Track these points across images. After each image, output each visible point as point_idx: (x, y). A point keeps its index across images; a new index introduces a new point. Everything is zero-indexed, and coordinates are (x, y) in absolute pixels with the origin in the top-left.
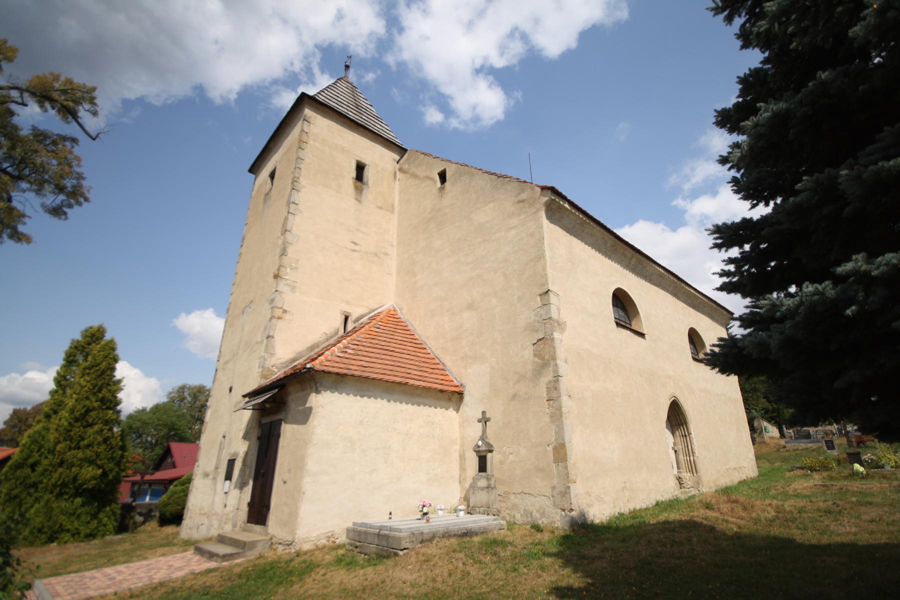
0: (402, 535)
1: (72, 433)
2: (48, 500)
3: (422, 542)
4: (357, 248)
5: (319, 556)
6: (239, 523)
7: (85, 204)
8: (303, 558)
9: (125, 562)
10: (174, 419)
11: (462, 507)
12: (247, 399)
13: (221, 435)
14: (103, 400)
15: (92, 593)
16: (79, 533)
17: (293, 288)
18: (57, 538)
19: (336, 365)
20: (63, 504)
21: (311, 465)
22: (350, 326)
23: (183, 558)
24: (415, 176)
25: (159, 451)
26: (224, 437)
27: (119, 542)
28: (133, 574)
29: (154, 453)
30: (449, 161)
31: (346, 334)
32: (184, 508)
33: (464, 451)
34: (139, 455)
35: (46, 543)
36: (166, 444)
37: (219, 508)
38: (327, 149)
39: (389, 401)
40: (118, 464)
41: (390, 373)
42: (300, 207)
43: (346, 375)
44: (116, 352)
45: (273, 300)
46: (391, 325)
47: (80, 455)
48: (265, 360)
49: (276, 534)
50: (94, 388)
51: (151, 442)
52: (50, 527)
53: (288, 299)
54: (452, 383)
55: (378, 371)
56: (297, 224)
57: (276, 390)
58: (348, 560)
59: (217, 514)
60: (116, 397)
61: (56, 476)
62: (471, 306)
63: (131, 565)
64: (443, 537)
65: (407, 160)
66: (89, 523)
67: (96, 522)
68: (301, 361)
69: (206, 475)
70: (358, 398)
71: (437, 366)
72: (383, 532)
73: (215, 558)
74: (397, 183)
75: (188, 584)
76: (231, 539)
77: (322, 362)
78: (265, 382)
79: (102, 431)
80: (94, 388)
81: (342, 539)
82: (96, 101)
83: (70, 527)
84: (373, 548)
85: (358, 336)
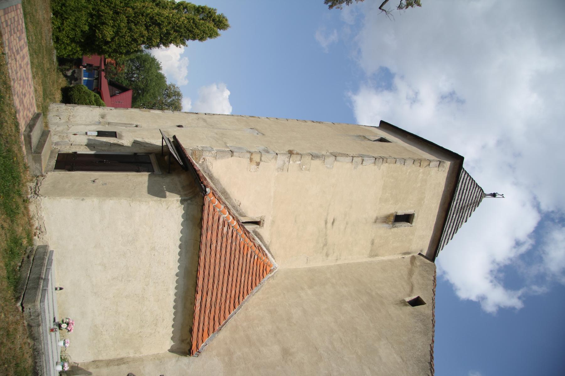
0: (38, 303)
1: (141, 17)
2: (87, 8)
3: (30, 326)
4: (329, 225)
5: (22, 221)
6: (59, 147)
7: (327, 6)
8: (22, 206)
9: (32, 63)
10: (152, 91)
11: (67, 368)
12: (172, 140)
13: (138, 124)
14: (168, 34)
15: (6, 37)
16: (60, 31)
17: (281, 169)
18: (57, 17)
19: (211, 217)
20: (84, 18)
21: (110, 204)
22: (249, 228)
23: (31, 104)
24: (411, 273)
25: (125, 83)
26: (137, 126)
27: (51, 60)
28: (21, 67)
29: (123, 80)
30: (434, 307)
31: (242, 225)
32: (75, 103)
33: (128, 362)
34: (122, 70)
35: (53, 10)
36: (130, 88)
37: (73, 130)
38: (419, 185)
39: (177, 275)
40: (115, 51)
41: (207, 273)
42: (360, 166)
43: (201, 227)
44: (208, 39)
45: (268, 152)
46: (256, 269)
47: (123, 25)
48: (210, 151)
49: (46, 179)
50: (177, 27)
51: (133, 77)
52: (65, 12)
53: (270, 166)
54: (200, 341)
55: (208, 260)
56: (343, 166)
57: (182, 163)
58: (16, 250)
59: (69, 128)
60: (171, 43)
61: (107, 10)
62: (286, 352)
63: (29, 66)
64: (34, 350)
65: (425, 263)
66: (68, 37)
67: (68, 42)
68: (211, 184)
69: (103, 117)
70: (179, 243)
71: (217, 323)
72: (42, 282)
73: (28, 129)
74: (400, 256)
75: (6, 109)
76: (45, 141)
77: (213, 203)
78: (189, 153)
79: (143, 37)
80: (177, 27)
81: (38, 242)
82: (410, 7)
83: (65, 24)
84: (26, 273)
85: (241, 236)
